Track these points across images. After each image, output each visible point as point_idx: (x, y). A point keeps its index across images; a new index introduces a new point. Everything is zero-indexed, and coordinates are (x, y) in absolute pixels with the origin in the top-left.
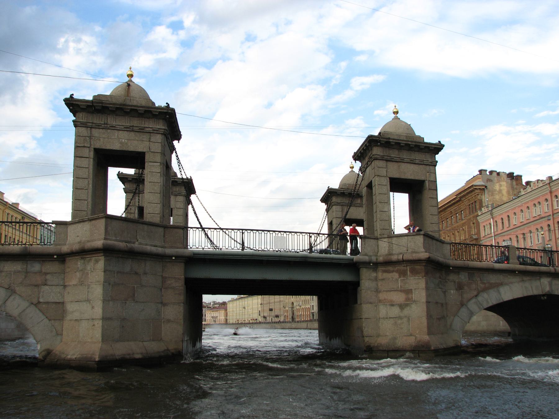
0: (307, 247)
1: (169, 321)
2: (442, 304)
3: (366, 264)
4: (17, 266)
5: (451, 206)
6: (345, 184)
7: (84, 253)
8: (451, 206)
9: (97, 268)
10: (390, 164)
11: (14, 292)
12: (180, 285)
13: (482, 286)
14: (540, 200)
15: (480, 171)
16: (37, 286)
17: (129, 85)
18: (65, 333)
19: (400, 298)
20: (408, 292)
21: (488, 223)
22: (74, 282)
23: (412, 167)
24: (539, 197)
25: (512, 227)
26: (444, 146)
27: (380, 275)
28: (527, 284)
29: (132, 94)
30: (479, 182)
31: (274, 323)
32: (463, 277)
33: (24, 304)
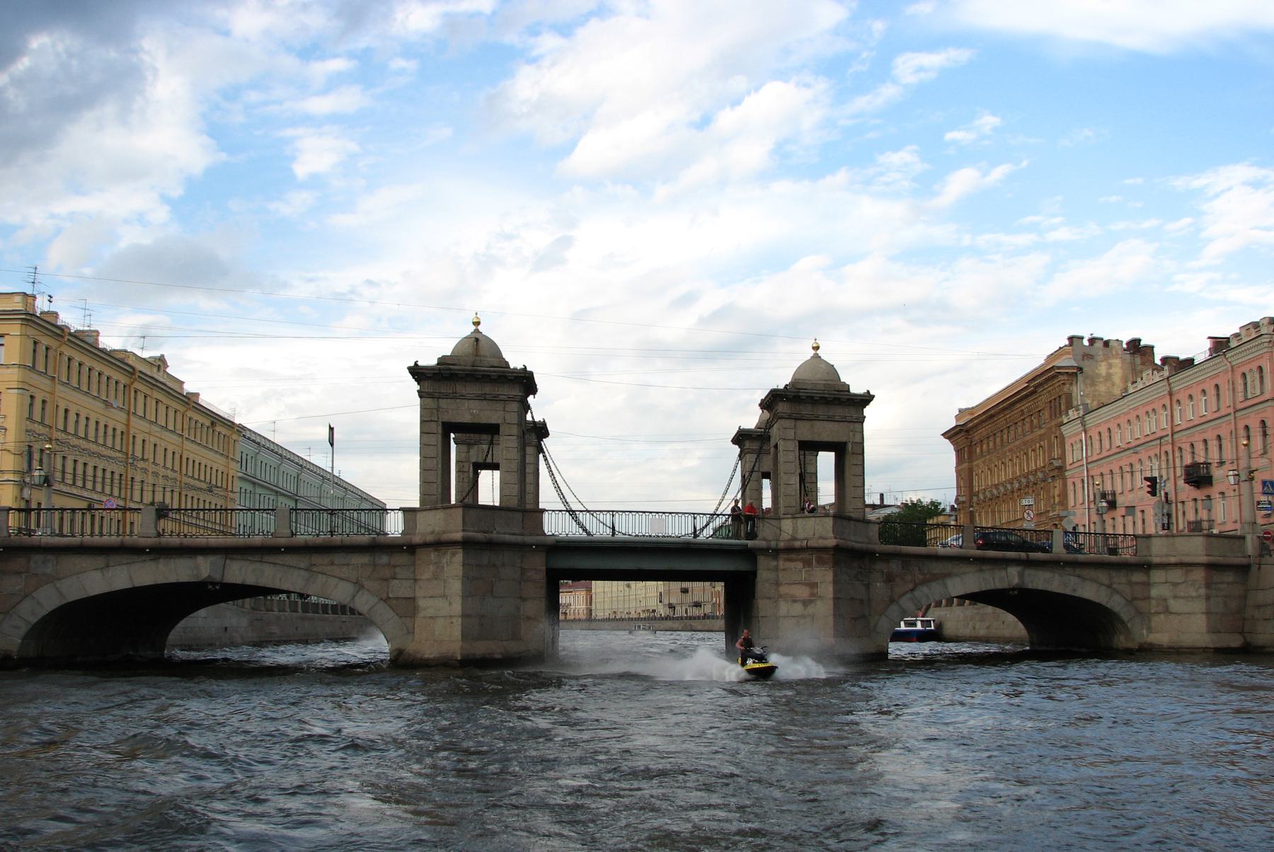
0: (690, 530)
2: (862, 601)
3: (764, 551)
4: (363, 559)
6: (805, 376)
7: (439, 545)
9: (454, 563)
10: (800, 423)
11: (362, 587)
12: (541, 577)
13: (921, 577)
14: (1155, 406)
15: (1071, 339)
16: (386, 580)
17: (477, 340)
19: (802, 592)
20: (813, 585)
21: (1254, 366)
22: (426, 576)
23: (830, 425)
24: (1152, 402)
25: (1114, 450)
26: (873, 397)
27: (781, 564)
29: (482, 352)
30: (1067, 361)
31: (690, 618)
32: (895, 566)
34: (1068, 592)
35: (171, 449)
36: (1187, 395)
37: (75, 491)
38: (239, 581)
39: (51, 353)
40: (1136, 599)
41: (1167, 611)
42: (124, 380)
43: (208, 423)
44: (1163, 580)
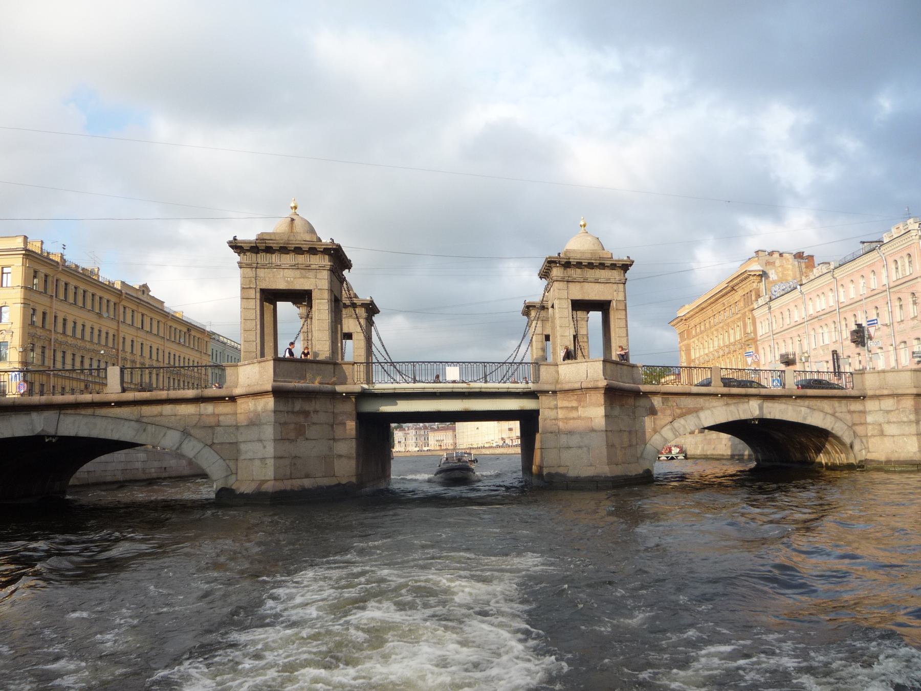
1: (340, 456)
5: (723, 296)
8: (723, 296)
10: (571, 285)
13: (678, 411)
16: (211, 427)
18: (239, 472)
28: (732, 408)
33: (199, 446)
34: (800, 420)
35: (161, 348)
36: (829, 288)
37: (74, 375)
38: (72, 434)
39: (50, 280)
40: (854, 424)
41: (882, 434)
42: (113, 299)
43: (185, 330)
44: (877, 408)
